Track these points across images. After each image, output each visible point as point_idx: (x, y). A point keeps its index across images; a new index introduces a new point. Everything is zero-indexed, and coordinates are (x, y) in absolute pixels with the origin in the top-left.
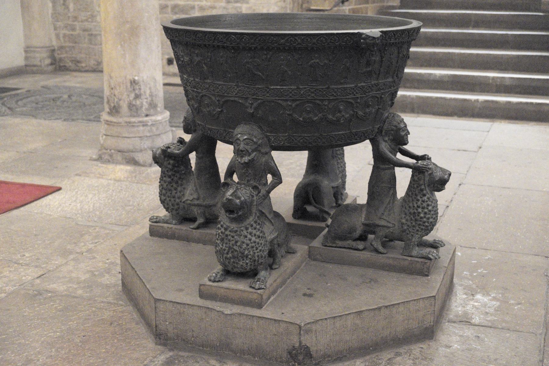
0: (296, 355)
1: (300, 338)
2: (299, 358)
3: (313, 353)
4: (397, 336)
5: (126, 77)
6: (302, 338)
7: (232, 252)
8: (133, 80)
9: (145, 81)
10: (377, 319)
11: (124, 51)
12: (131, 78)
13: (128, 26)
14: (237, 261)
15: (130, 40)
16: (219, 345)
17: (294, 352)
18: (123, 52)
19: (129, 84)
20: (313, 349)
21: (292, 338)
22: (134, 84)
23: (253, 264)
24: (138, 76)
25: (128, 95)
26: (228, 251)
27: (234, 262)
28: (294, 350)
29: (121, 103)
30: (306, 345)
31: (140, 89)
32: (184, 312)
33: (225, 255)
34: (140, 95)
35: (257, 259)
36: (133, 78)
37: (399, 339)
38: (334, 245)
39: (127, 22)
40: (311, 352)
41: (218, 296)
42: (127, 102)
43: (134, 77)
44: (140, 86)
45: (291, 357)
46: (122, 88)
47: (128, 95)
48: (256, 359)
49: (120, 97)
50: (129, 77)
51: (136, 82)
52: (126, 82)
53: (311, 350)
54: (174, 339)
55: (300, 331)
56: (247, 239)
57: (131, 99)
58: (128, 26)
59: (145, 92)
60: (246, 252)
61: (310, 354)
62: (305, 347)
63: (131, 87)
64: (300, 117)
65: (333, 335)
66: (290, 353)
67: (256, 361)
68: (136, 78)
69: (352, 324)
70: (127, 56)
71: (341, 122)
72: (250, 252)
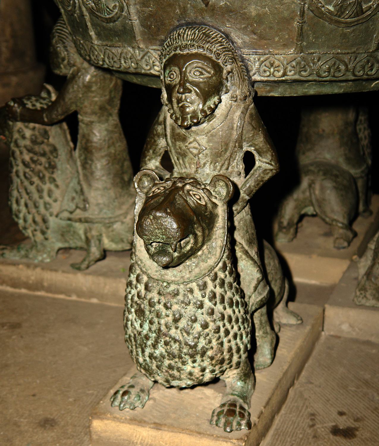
14: (180, 365)
27: (170, 367)
33: (148, 351)
72: (210, 342)
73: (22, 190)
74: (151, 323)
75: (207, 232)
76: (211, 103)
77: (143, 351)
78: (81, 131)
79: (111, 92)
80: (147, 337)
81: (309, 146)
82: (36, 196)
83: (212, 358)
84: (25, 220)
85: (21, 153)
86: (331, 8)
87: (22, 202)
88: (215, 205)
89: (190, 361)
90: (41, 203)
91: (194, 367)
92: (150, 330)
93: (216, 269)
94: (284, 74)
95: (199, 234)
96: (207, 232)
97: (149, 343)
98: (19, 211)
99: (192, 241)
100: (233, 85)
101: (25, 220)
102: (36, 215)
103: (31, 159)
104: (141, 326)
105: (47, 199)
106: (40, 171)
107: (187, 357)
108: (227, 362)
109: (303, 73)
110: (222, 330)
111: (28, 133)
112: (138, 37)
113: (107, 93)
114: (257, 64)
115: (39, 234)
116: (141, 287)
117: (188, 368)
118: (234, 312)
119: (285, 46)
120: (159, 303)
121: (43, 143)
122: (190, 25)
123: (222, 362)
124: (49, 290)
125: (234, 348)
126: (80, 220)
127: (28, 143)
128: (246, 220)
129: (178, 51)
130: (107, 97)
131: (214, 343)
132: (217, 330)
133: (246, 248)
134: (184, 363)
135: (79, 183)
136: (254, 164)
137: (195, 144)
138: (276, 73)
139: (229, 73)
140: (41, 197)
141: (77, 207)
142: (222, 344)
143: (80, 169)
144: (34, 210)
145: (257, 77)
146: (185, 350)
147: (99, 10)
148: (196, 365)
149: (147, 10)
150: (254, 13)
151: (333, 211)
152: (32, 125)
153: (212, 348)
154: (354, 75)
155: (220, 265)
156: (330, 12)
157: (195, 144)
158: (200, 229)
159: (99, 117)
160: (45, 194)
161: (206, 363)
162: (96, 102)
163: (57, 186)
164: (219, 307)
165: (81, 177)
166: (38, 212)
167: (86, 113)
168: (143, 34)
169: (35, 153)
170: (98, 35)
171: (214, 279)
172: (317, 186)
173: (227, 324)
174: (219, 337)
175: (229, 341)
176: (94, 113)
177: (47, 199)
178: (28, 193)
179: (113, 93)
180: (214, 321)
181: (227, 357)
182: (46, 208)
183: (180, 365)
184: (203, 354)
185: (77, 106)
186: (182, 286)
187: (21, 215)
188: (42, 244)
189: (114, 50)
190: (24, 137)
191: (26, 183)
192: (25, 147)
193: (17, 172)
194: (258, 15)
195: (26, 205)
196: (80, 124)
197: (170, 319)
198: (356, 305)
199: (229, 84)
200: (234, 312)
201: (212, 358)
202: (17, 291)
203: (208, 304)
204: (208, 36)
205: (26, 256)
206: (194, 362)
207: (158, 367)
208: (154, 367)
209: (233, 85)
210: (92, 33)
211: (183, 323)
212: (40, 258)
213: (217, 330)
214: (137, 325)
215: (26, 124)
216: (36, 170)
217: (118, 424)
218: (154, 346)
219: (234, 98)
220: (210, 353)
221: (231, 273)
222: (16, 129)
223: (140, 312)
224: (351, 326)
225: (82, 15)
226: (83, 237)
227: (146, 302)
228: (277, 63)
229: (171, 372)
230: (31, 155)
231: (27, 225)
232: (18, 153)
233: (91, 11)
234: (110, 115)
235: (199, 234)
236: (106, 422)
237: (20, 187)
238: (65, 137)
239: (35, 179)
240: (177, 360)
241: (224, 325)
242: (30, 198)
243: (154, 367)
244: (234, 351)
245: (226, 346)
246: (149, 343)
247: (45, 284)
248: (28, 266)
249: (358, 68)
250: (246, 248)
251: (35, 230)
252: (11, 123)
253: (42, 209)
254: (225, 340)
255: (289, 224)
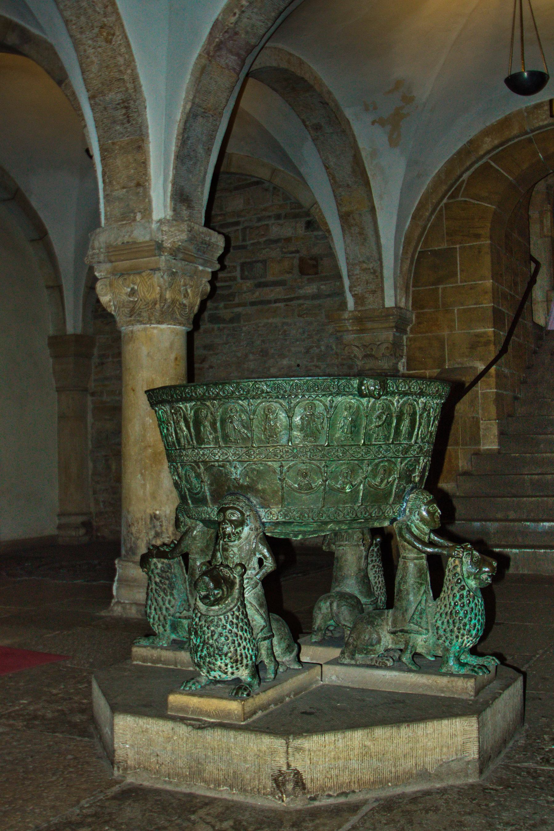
0: (284, 784)
1: (287, 758)
2: (287, 787)
3: (309, 785)
4: (426, 770)
5: (145, 511)
6: (290, 759)
7: (207, 648)
8: (153, 515)
9: (167, 516)
10: (395, 742)
11: (144, 480)
12: (151, 512)
13: (150, 450)
14: (214, 661)
15: (152, 467)
16: (189, 774)
17: (280, 778)
18: (143, 482)
19: (148, 520)
20: (306, 777)
21: (277, 759)
22: (155, 521)
23: (234, 665)
24: (160, 510)
25: (147, 533)
26: (203, 648)
27: (209, 662)
28: (281, 776)
29: (139, 542)
30: (296, 769)
31: (161, 526)
32: (147, 729)
33: (199, 654)
34: (162, 532)
35: (239, 659)
36: (154, 513)
37: (430, 773)
38: (353, 662)
39: (150, 446)
40: (304, 781)
41: (190, 708)
42: (145, 542)
43: (154, 511)
44: (162, 522)
45: (278, 786)
46: (140, 524)
47: (147, 533)
48: (235, 792)
49: (138, 535)
50: (149, 511)
51: (157, 517)
52: (145, 519)
53: (304, 778)
54: (135, 768)
55: (288, 747)
56: (227, 630)
57: (151, 537)
58: (150, 450)
59: (167, 530)
60: (225, 649)
61: (302, 782)
62: (296, 772)
63: (151, 523)
64: (295, 484)
65: (334, 758)
66: (276, 780)
67: (234, 794)
68: (158, 512)
69: (361, 745)
70: (148, 486)
71: (347, 491)
72: (230, 648)
73: (154, 601)
74: (201, 638)
75: (229, 590)
76: (238, 530)
77: (197, 655)
78: (190, 564)
79: (207, 541)
80: (199, 646)
81: (337, 584)
82: (161, 603)
83: (231, 658)
84: (154, 619)
85: (155, 577)
86: (296, 486)
87: (153, 607)
88: (235, 578)
89: (219, 659)
90: (164, 607)
91: (221, 663)
92: (200, 642)
93: (234, 610)
94: (277, 519)
95: (225, 590)
96: (229, 590)
97: (200, 649)
98: (151, 613)
99: (221, 593)
100: (250, 522)
101: (154, 619)
102: (161, 615)
103: (160, 581)
104: (196, 641)
105: (168, 606)
106: (165, 589)
107: (218, 656)
108: (239, 662)
109: (287, 518)
110: (236, 642)
111: (159, 565)
112: (209, 501)
113: (205, 541)
114: (264, 513)
115: (161, 627)
116: (197, 620)
117: (218, 663)
118: (244, 634)
119: (277, 504)
120: (205, 626)
121: (168, 571)
122: (231, 494)
123: (236, 661)
124: (164, 663)
125: (244, 655)
126: (185, 618)
127: (159, 571)
128: (258, 594)
129: (224, 506)
130: (205, 545)
131: (232, 649)
132: (233, 642)
133: (258, 608)
134: (216, 660)
135: (187, 595)
136: (263, 563)
137: (232, 552)
138: (274, 518)
139: (248, 516)
140: (164, 604)
141: (184, 609)
142: (236, 650)
143: (188, 587)
144: (159, 613)
145: (264, 520)
146: (216, 652)
147: (192, 489)
148: (222, 661)
149: (213, 488)
150: (260, 488)
151: (345, 620)
152: (162, 560)
153: (231, 652)
154: (313, 520)
155: (236, 607)
156: (296, 488)
157: (232, 552)
158: (225, 587)
159: (200, 556)
160: (167, 602)
161: (227, 661)
162: (199, 547)
163: (174, 598)
164: (235, 630)
165: (188, 591)
166: (162, 613)
167: (193, 553)
168: (211, 500)
169: (163, 577)
170: (192, 502)
171: (232, 615)
172: (335, 605)
173: (239, 640)
174: (235, 646)
175: (241, 650)
176: (197, 553)
177: (168, 606)
178: (156, 602)
179: (209, 542)
180: (232, 636)
181: (239, 659)
182: (166, 611)
183: (214, 661)
184: (226, 655)
185: (187, 549)
186: (216, 617)
187: (152, 616)
188: (163, 634)
189: (199, 509)
190: (157, 568)
191: (156, 596)
192: (157, 573)
193: (152, 589)
194: (262, 489)
195: (155, 609)
196: (190, 560)
197: (210, 634)
198: (338, 663)
199: (248, 522)
200: (244, 634)
201: (231, 658)
202: (145, 664)
203: (229, 627)
204: (239, 499)
205: (153, 643)
206: (221, 659)
207: (204, 663)
208: (202, 664)
209: (250, 522)
210: (190, 501)
211: (215, 637)
212: (161, 644)
213: (233, 642)
214: (194, 641)
215: (159, 559)
216: (163, 588)
217: (182, 696)
218: (202, 651)
219: (251, 529)
220: (229, 655)
221: (243, 613)
222: (153, 563)
223: (196, 633)
224: (337, 677)
225: (185, 492)
226: (187, 629)
227: (199, 627)
228: (273, 512)
229: (210, 666)
230: (160, 578)
231: (155, 622)
232: (153, 577)
233: (189, 490)
234: (207, 555)
235: (225, 590)
236: (176, 696)
237: (152, 598)
238: (182, 570)
239: (162, 594)
240: (213, 658)
241: (238, 640)
242: (158, 605)
243: (202, 664)
244: (244, 657)
245: (239, 652)
246: (200, 649)
247: (163, 659)
248: (153, 648)
249: (314, 516)
250: (258, 608)
251: (159, 625)
252: (150, 560)
253: (164, 612)
254: (238, 649)
255: (317, 629)
